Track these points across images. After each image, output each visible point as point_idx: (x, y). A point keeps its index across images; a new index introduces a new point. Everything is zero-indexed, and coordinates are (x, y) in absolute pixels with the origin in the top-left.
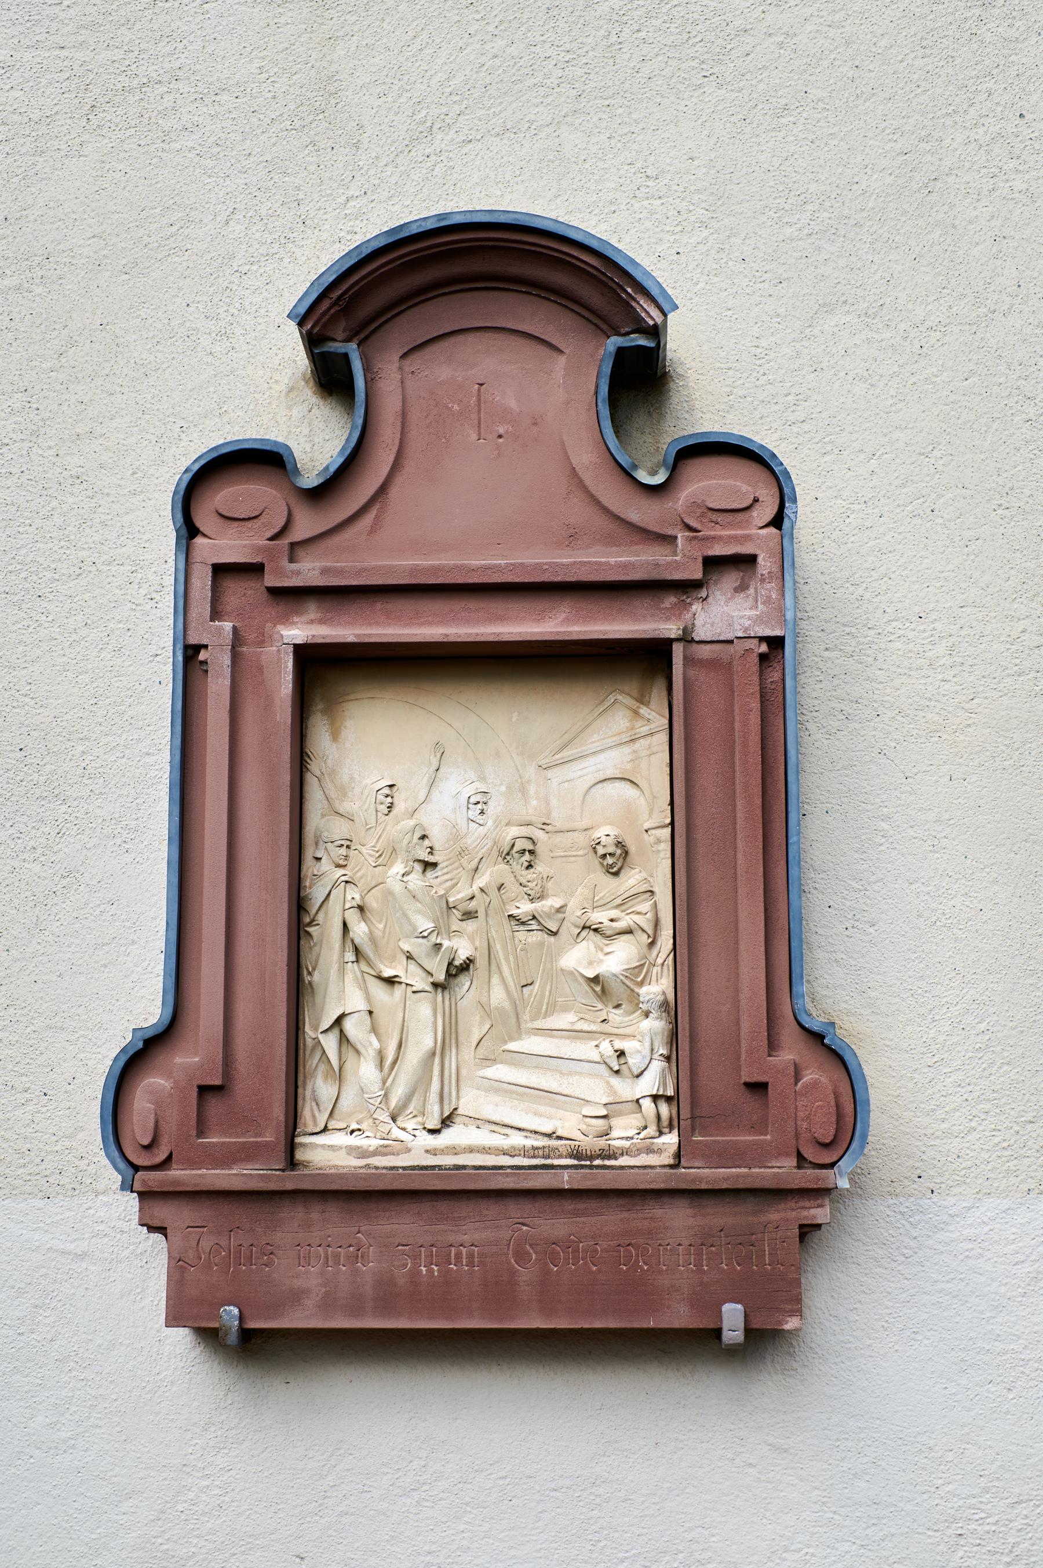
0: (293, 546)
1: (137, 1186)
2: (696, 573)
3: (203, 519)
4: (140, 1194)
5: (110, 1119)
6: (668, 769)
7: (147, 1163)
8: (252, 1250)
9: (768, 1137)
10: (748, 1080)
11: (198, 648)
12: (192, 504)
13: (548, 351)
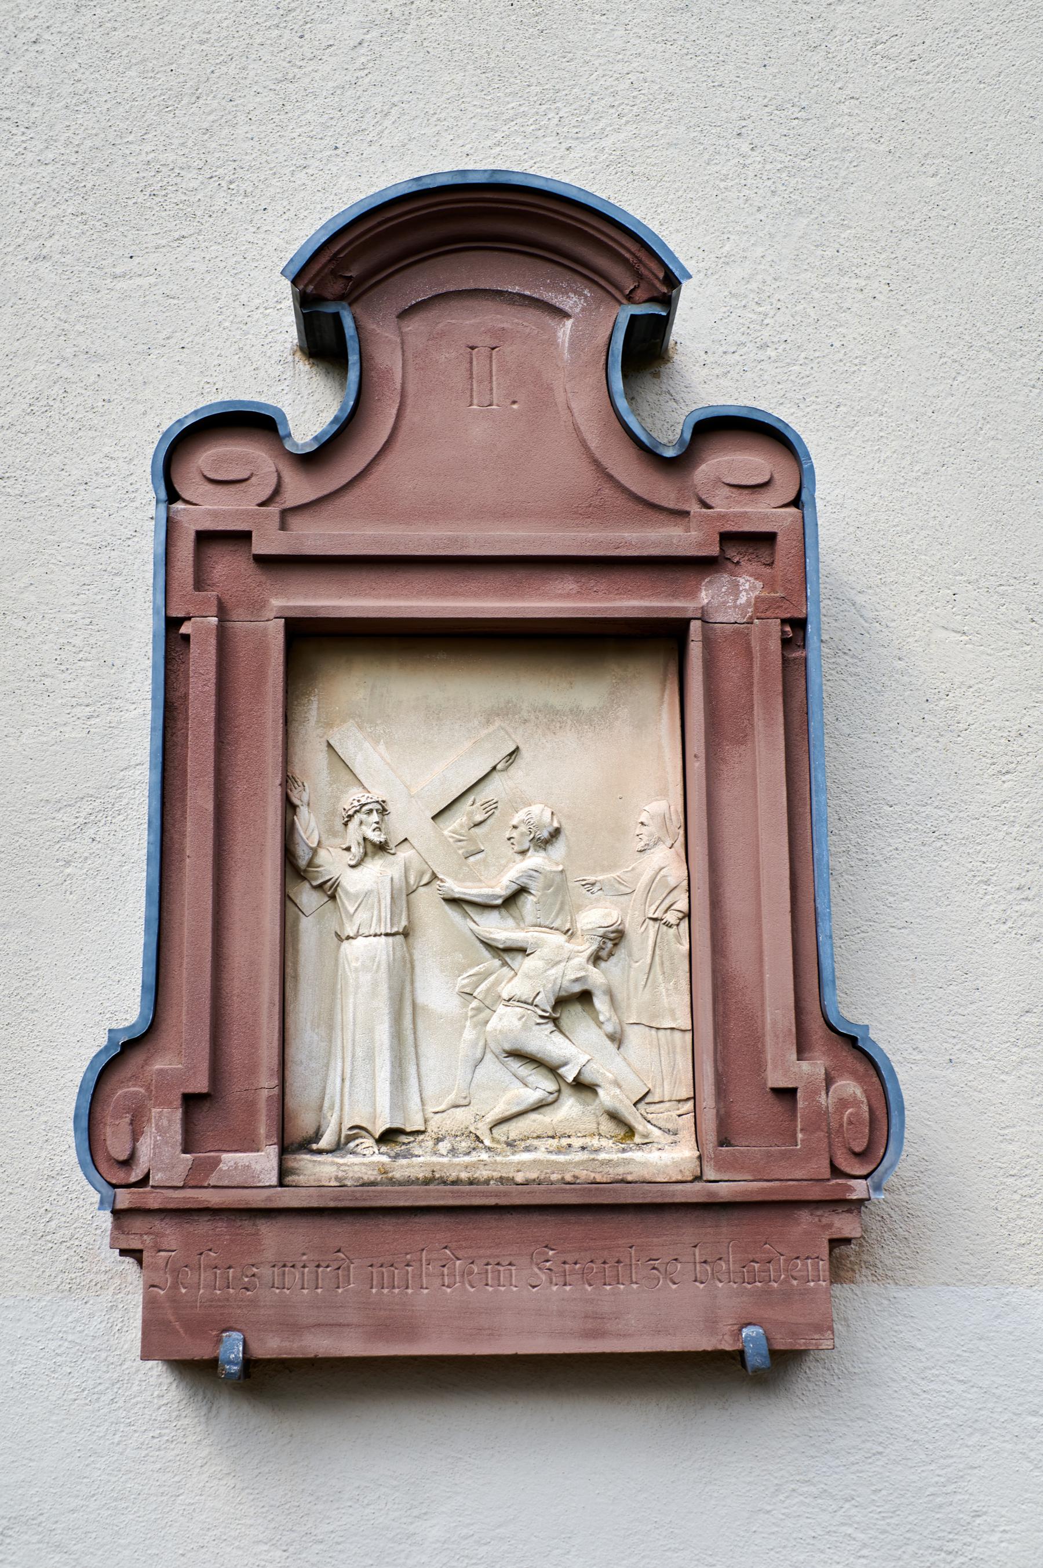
0: (285, 513)
3: (190, 486)
6: (688, 974)
8: (216, 1273)
10: (776, 1086)
12: (172, 468)
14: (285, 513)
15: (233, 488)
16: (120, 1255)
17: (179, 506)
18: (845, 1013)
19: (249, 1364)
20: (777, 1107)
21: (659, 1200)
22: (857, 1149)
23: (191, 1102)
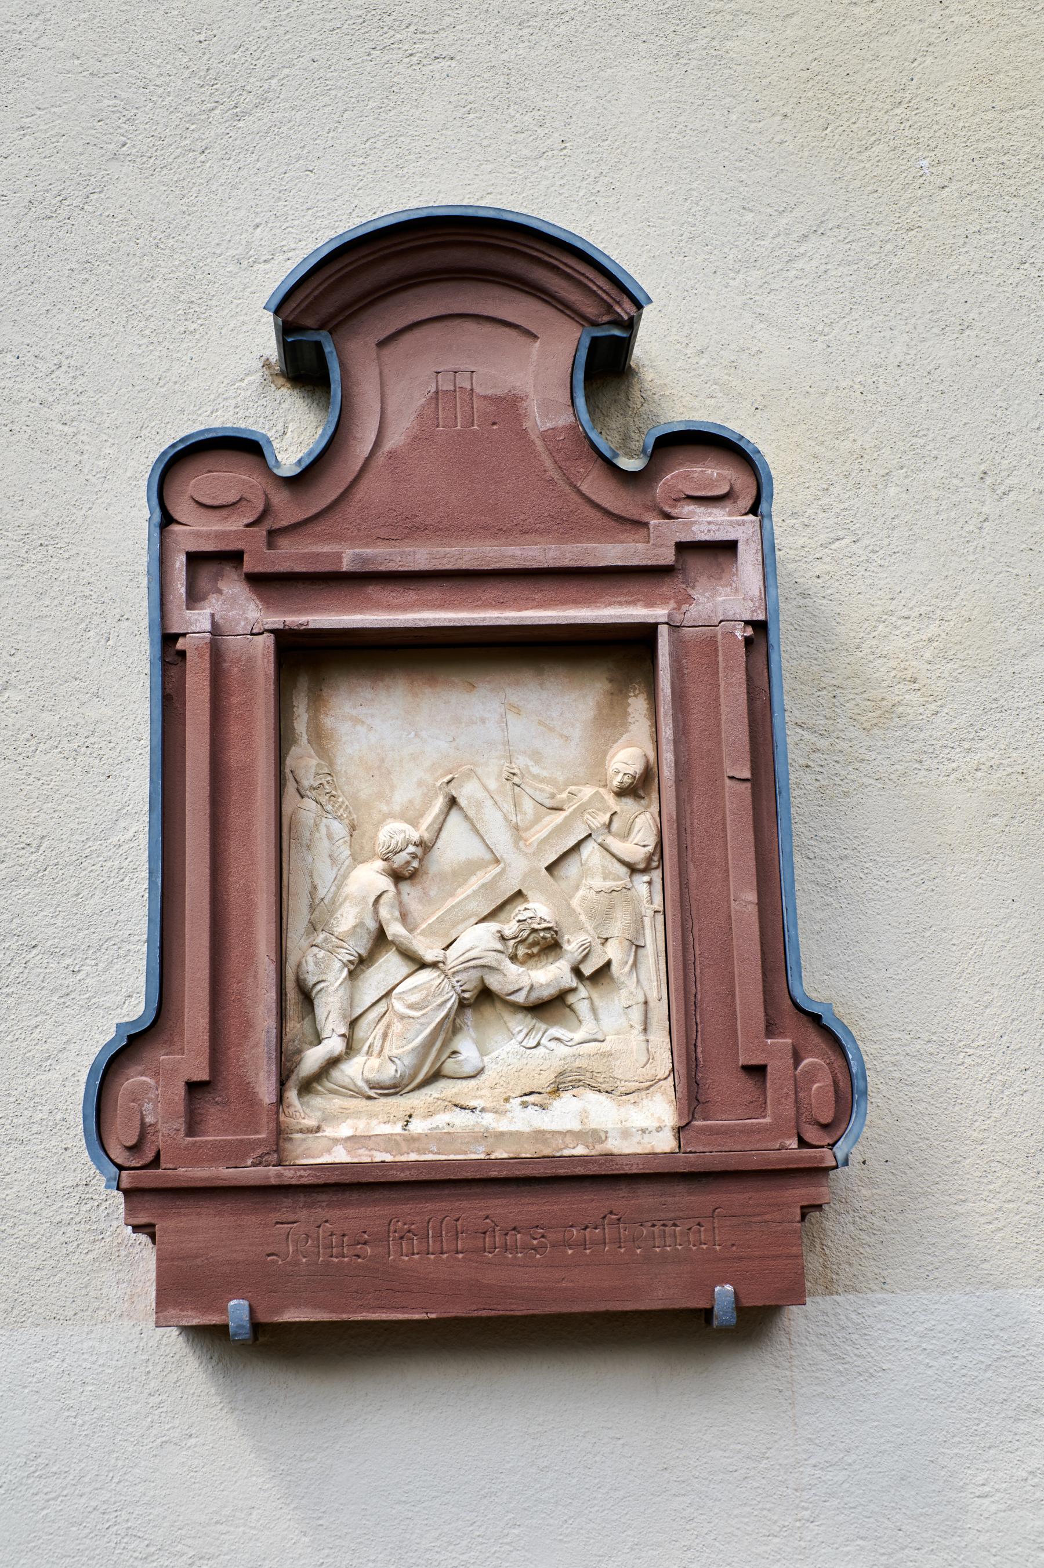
1: (124, 1185)
2: (668, 556)
3: (182, 510)
5: (333, 1179)
7: (134, 1164)
9: (768, 1120)
11: (176, 637)
13: (522, 339)
14: (272, 534)
16: (134, 1233)
17: (176, 528)
18: (813, 995)
19: (257, 1327)
20: (747, 1083)
22: (823, 1121)
23: (193, 1088)
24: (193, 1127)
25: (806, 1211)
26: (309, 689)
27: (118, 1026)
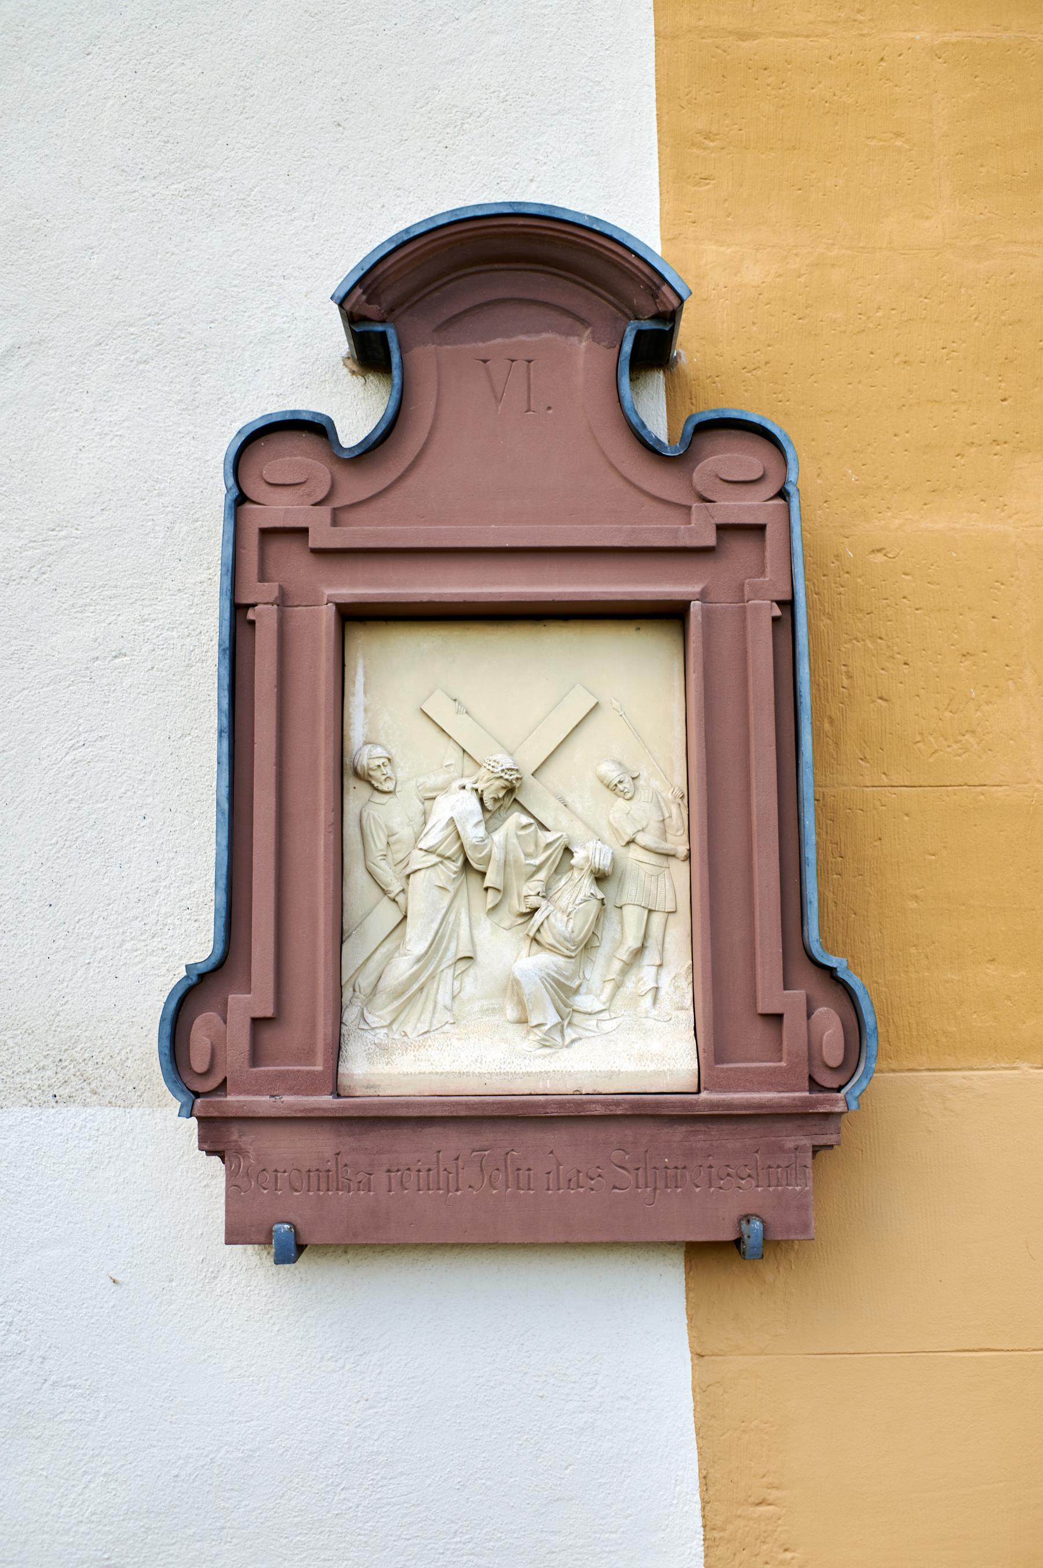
2: (709, 539)
4: (197, 1118)
9: (783, 1064)
14: (335, 511)
15: (291, 489)
17: (248, 506)
21: (251, 1115)
23: (258, 1023)
24: (255, 1058)
25: (816, 1150)
26: (685, 1252)
27: (188, 967)
